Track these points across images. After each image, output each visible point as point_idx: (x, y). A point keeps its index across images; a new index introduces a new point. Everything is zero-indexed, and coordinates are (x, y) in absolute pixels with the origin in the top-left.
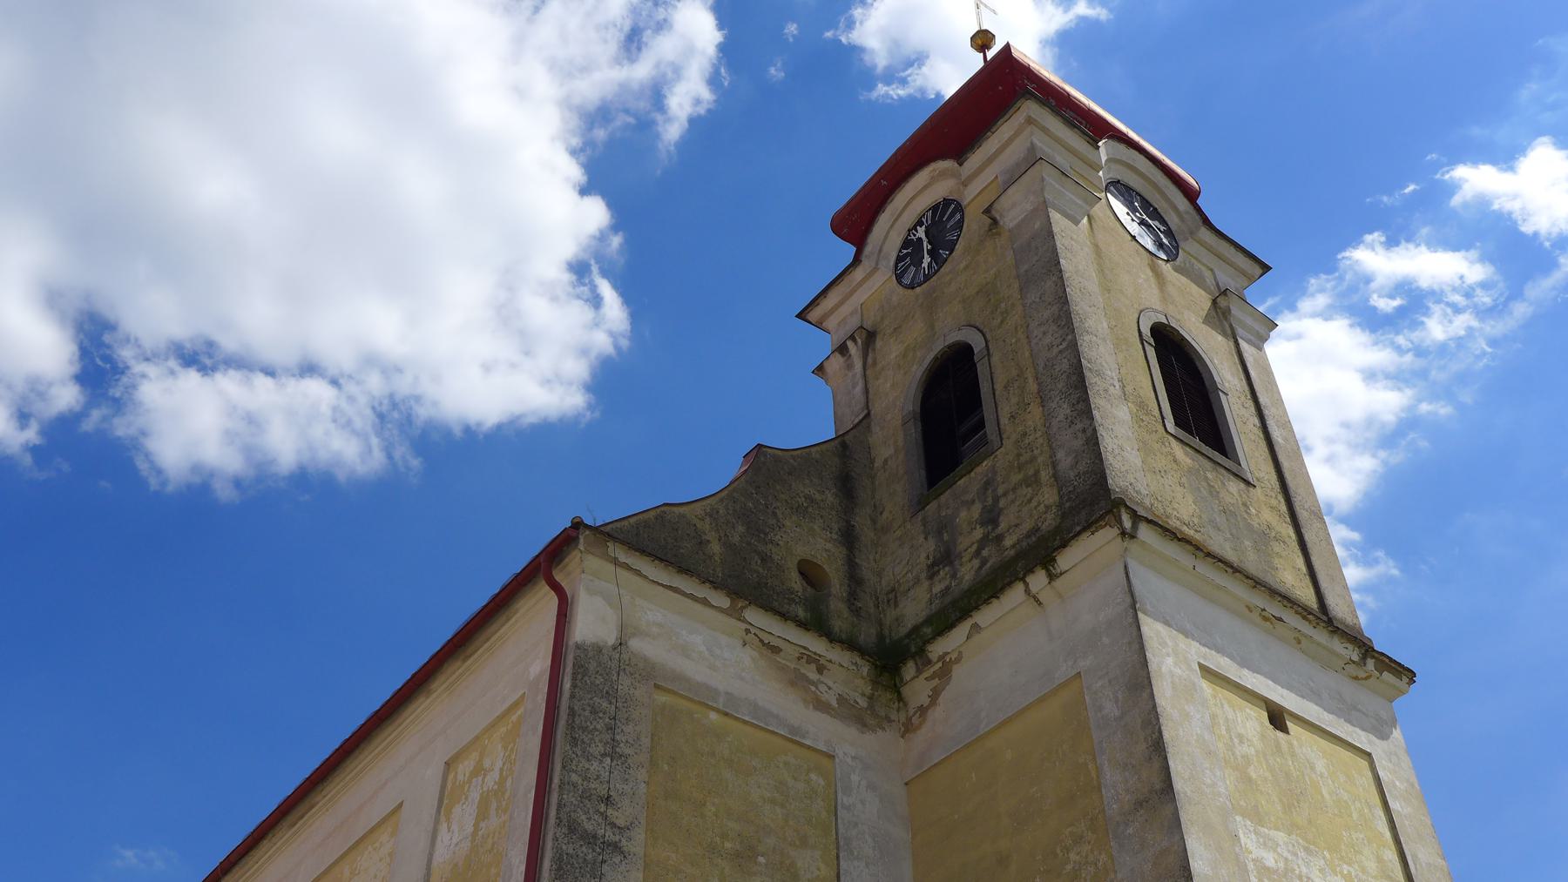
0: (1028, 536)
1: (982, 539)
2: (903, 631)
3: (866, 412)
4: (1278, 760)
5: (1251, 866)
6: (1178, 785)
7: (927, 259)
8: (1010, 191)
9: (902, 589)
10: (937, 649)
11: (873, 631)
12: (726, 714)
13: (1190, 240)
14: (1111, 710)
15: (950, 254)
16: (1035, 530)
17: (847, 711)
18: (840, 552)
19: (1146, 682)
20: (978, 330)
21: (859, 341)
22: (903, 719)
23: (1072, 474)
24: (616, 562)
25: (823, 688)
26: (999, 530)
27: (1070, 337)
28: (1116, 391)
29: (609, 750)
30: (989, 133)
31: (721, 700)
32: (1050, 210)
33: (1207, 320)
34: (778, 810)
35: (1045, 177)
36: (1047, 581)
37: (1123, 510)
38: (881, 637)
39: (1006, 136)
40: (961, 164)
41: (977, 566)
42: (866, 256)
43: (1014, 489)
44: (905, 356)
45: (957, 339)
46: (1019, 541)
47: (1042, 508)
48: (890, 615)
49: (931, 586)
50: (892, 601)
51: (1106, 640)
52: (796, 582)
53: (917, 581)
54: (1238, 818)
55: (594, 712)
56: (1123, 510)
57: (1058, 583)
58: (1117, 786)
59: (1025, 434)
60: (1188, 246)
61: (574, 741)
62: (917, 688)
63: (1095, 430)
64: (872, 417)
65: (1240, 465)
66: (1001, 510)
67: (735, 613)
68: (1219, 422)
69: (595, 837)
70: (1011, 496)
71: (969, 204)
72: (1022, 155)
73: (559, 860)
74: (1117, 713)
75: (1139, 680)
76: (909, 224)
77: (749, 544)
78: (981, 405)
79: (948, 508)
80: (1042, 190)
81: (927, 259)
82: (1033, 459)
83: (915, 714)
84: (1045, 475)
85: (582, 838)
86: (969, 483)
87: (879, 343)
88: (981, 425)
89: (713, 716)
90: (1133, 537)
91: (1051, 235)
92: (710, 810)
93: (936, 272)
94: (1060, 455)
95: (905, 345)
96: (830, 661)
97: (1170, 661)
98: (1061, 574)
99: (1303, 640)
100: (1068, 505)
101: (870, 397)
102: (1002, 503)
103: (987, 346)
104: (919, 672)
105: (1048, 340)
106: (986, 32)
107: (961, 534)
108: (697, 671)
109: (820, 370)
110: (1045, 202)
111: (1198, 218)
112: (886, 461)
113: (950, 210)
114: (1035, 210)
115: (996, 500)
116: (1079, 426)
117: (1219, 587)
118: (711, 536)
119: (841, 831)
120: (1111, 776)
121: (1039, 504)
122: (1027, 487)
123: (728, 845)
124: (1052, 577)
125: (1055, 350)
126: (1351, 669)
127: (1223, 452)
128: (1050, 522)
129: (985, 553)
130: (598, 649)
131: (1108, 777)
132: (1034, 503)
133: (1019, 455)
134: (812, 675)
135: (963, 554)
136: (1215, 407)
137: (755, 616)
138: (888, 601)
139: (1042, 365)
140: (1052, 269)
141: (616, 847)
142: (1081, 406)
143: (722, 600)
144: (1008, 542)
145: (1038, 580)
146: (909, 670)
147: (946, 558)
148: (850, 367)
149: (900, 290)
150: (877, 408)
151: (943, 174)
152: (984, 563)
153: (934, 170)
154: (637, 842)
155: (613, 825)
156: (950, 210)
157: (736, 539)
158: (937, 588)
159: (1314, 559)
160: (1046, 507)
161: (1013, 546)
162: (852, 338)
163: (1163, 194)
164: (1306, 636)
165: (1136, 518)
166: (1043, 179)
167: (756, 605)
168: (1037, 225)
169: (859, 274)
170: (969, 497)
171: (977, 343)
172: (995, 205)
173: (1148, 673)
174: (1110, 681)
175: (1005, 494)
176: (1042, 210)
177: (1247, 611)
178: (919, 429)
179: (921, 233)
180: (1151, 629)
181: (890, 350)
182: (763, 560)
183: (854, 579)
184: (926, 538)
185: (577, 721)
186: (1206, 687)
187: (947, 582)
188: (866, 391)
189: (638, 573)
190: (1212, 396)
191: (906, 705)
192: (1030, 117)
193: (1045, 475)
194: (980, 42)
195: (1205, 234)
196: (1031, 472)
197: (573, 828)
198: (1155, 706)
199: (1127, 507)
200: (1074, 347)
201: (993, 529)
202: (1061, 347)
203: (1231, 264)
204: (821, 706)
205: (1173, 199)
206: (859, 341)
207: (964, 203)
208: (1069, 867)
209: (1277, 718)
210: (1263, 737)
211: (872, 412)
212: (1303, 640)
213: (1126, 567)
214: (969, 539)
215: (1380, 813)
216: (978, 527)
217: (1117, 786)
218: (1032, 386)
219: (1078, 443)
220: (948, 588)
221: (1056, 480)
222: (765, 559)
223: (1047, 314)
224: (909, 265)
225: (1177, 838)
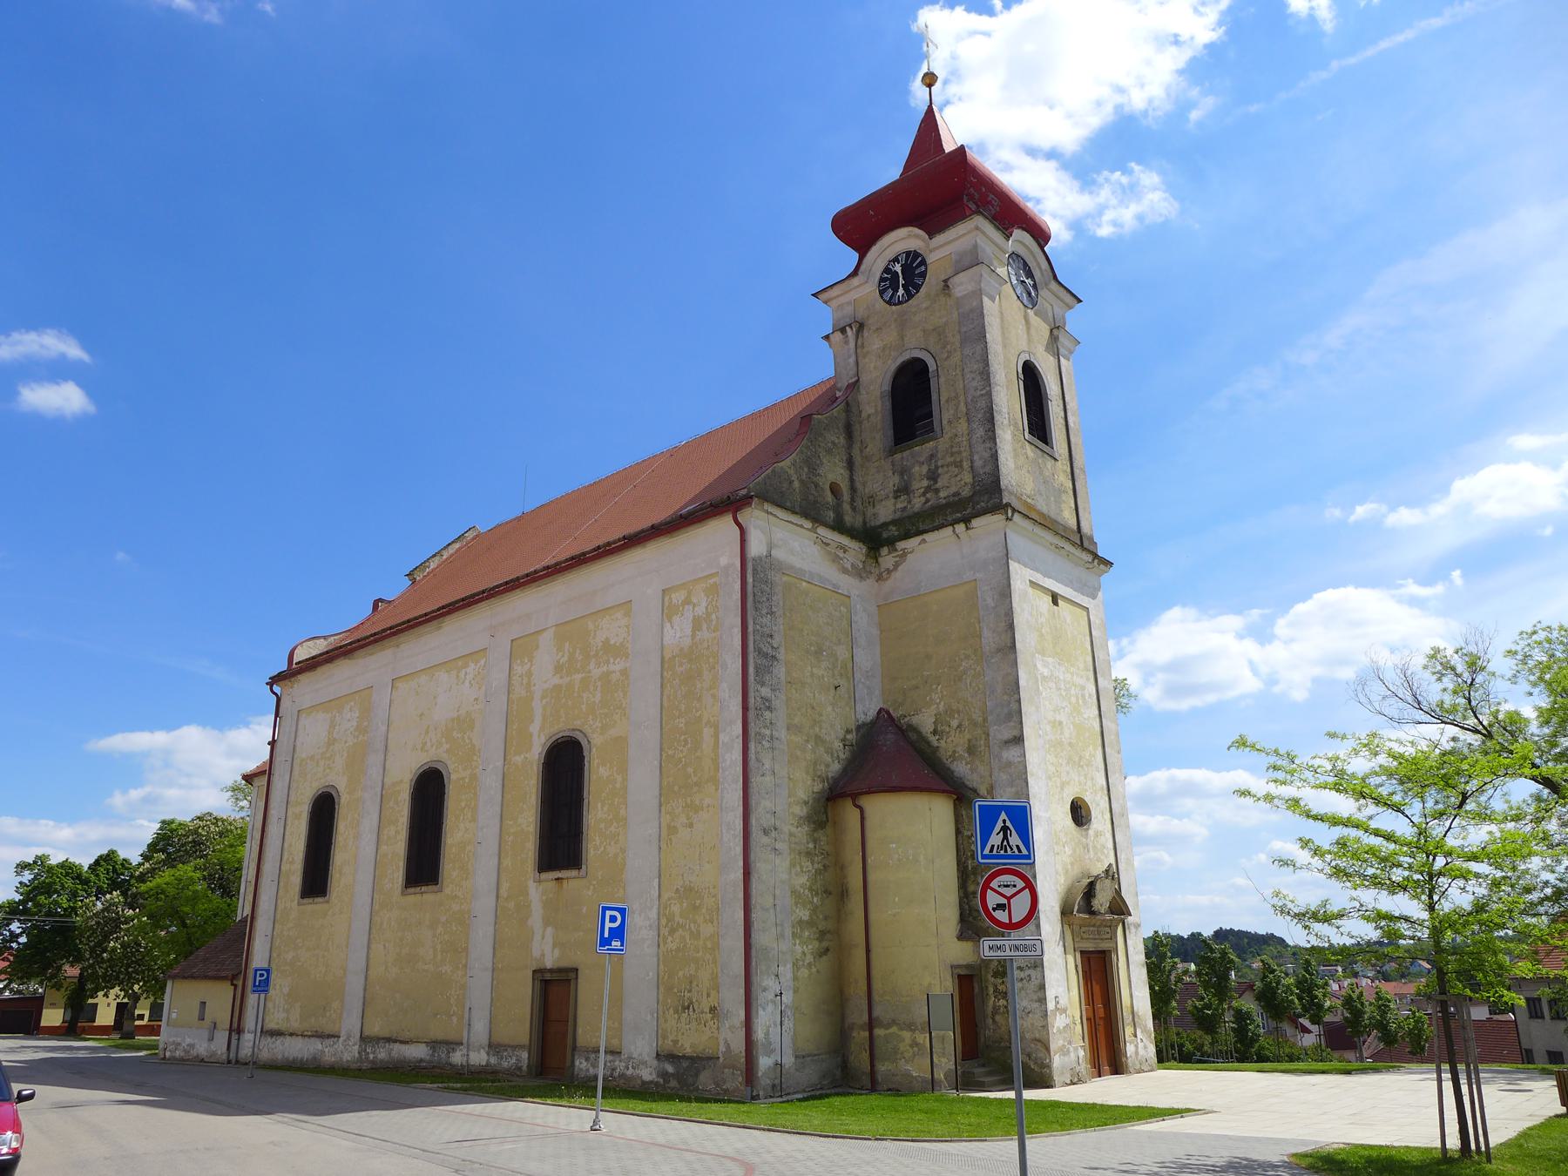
0: (954, 495)
1: (928, 487)
3: (857, 378)
5: (1039, 677)
6: (1018, 645)
7: (901, 291)
8: (961, 275)
10: (901, 545)
11: (861, 520)
13: (1045, 289)
15: (917, 293)
16: (956, 494)
17: (860, 573)
18: (846, 474)
21: (854, 329)
26: (937, 486)
28: (1006, 422)
33: (1047, 349)
38: (865, 523)
39: (961, 233)
40: (931, 239)
43: (948, 466)
46: (948, 496)
47: (963, 482)
48: (870, 511)
51: (991, 568)
53: (887, 497)
58: (989, 639)
60: (1043, 293)
61: (756, 609)
62: (887, 559)
63: (996, 451)
67: (813, 530)
70: (946, 469)
74: (993, 605)
76: (892, 256)
80: (980, 281)
82: (960, 453)
84: (966, 465)
86: (923, 450)
87: (866, 334)
88: (930, 415)
89: (804, 584)
90: (1011, 520)
92: (1186, 972)
93: (907, 301)
94: (976, 457)
97: (1019, 582)
100: (978, 488)
102: (940, 471)
104: (890, 553)
105: (975, 384)
106: (933, 74)
107: (915, 479)
108: (796, 562)
109: (827, 338)
111: (1051, 274)
113: (918, 261)
114: (973, 292)
115: (937, 467)
116: (988, 445)
118: (794, 478)
120: (986, 633)
121: (961, 480)
124: (967, 528)
125: (979, 393)
129: (928, 495)
130: (760, 558)
132: (958, 478)
134: (841, 555)
136: (1045, 409)
138: (869, 502)
141: (774, 657)
142: (990, 433)
143: (808, 524)
144: (942, 494)
145: (960, 528)
146: (885, 551)
148: (846, 343)
149: (881, 304)
150: (864, 378)
151: (917, 236)
152: (927, 501)
153: (912, 231)
154: (781, 655)
156: (918, 261)
157: (804, 477)
158: (900, 506)
160: (965, 483)
162: (850, 326)
165: (1014, 510)
166: (981, 275)
168: (975, 304)
169: (855, 281)
170: (922, 459)
171: (932, 366)
175: (942, 466)
179: (898, 268)
180: (1013, 566)
183: (853, 489)
184: (894, 474)
186: (1030, 590)
187: (906, 504)
188: (857, 363)
189: (775, 516)
193: (966, 465)
195: (1053, 285)
196: (958, 460)
197: (759, 651)
200: (989, 395)
203: (1062, 301)
204: (845, 571)
206: (854, 329)
207: (928, 262)
208: (961, 668)
213: (1005, 534)
214: (920, 485)
217: (989, 639)
218: (963, 408)
219: (987, 455)
220: (905, 507)
222: (816, 486)
224: (888, 288)
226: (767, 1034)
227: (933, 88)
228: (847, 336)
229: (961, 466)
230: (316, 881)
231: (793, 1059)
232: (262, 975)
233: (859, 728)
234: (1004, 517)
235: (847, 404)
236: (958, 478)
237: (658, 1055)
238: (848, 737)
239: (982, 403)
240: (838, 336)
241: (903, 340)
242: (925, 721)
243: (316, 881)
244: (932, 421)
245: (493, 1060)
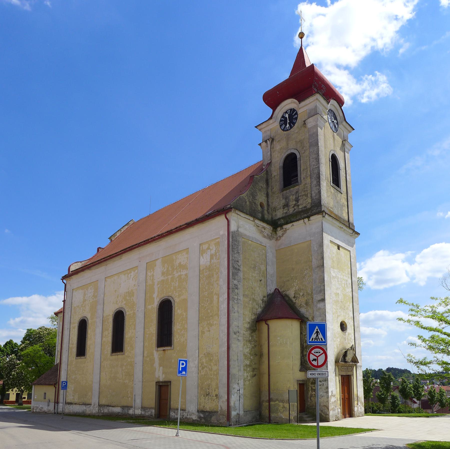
2: (277, 218)
3: (271, 161)
7: (288, 125)
8: (310, 118)
9: (277, 208)
10: (285, 227)
11: (271, 217)
12: (252, 241)
14: (316, 249)
16: (305, 207)
18: (266, 199)
19: (322, 246)
20: (298, 152)
21: (270, 141)
22: (276, 237)
23: (315, 198)
24: (237, 214)
25: (265, 233)
26: (298, 204)
27: (318, 165)
30: (307, 99)
31: (251, 238)
32: (318, 127)
34: (259, 258)
35: (318, 118)
36: (308, 221)
37: (324, 212)
38: (272, 218)
39: (311, 101)
41: (293, 210)
42: (274, 118)
44: (281, 149)
45: (294, 152)
46: (302, 208)
49: (283, 210)
50: (275, 210)
51: (317, 235)
53: (280, 208)
54: (331, 268)
56: (324, 212)
57: (309, 221)
58: (315, 263)
59: (306, 184)
61: (233, 251)
62: (280, 232)
63: (320, 190)
64: (272, 163)
65: (341, 189)
66: (299, 199)
67: (254, 221)
68: (339, 184)
70: (302, 197)
71: (299, 114)
72: (314, 107)
73: (233, 273)
75: (321, 245)
79: (288, 194)
80: (317, 121)
81: (288, 125)
82: (307, 191)
83: (279, 237)
84: (309, 195)
86: (294, 189)
89: (250, 242)
91: (317, 135)
93: (290, 129)
94: (313, 192)
95: (281, 147)
96: (266, 228)
97: (326, 241)
98: (311, 220)
99: (345, 231)
100: (313, 204)
101: (272, 157)
102: (300, 198)
103: (300, 157)
104: (281, 230)
105: (314, 163)
107: (290, 201)
108: (247, 233)
109: (260, 144)
110: (317, 125)
111: (344, 118)
112: (275, 176)
114: (315, 126)
115: (299, 197)
116: (317, 188)
118: (247, 200)
119: (267, 261)
120: (314, 260)
122: (305, 196)
123: (252, 266)
124: (309, 220)
125: (315, 167)
126: (351, 234)
127: (339, 187)
128: (309, 206)
129: (295, 207)
130: (235, 232)
131: (313, 260)
132: (306, 201)
133: (304, 188)
135: (291, 206)
138: (274, 210)
139: (312, 169)
140: (317, 145)
142: (318, 183)
144: (300, 207)
145: (306, 220)
146: (279, 229)
147: (286, 205)
148: (267, 146)
150: (273, 161)
151: (294, 102)
152: (295, 210)
155: (238, 266)
158: (285, 211)
159: (349, 209)
161: (301, 208)
162: (269, 140)
163: (338, 111)
164: (345, 230)
165: (326, 213)
166: (318, 119)
167: (257, 219)
169: (271, 121)
172: (306, 121)
173: (323, 244)
174: (316, 243)
175: (301, 196)
176: (316, 126)
177: (338, 227)
179: (287, 116)
181: (278, 146)
182: (255, 204)
183: (268, 205)
184: (283, 199)
187: (287, 211)
190: (338, 170)
191: (277, 234)
192: (317, 98)
193: (309, 195)
194: (301, 36)
195: (344, 123)
196: (306, 193)
198: (323, 251)
199: (325, 212)
200: (319, 167)
201: (297, 203)
202: (316, 167)
204: (264, 237)
205: (340, 113)
206: (270, 141)
209: (339, 247)
211: (272, 161)
212: (345, 231)
215: (350, 262)
216: (294, 201)
217: (315, 263)
219: (317, 191)
220: (287, 212)
221: (311, 197)
223: (314, 156)
224: (283, 124)
225: (323, 274)
231: (243, 412)
232: (64, 384)
233: (268, 295)
235: (267, 171)
237: (198, 411)
238: (264, 299)
239: (316, 171)
242: (291, 293)
245: (143, 413)
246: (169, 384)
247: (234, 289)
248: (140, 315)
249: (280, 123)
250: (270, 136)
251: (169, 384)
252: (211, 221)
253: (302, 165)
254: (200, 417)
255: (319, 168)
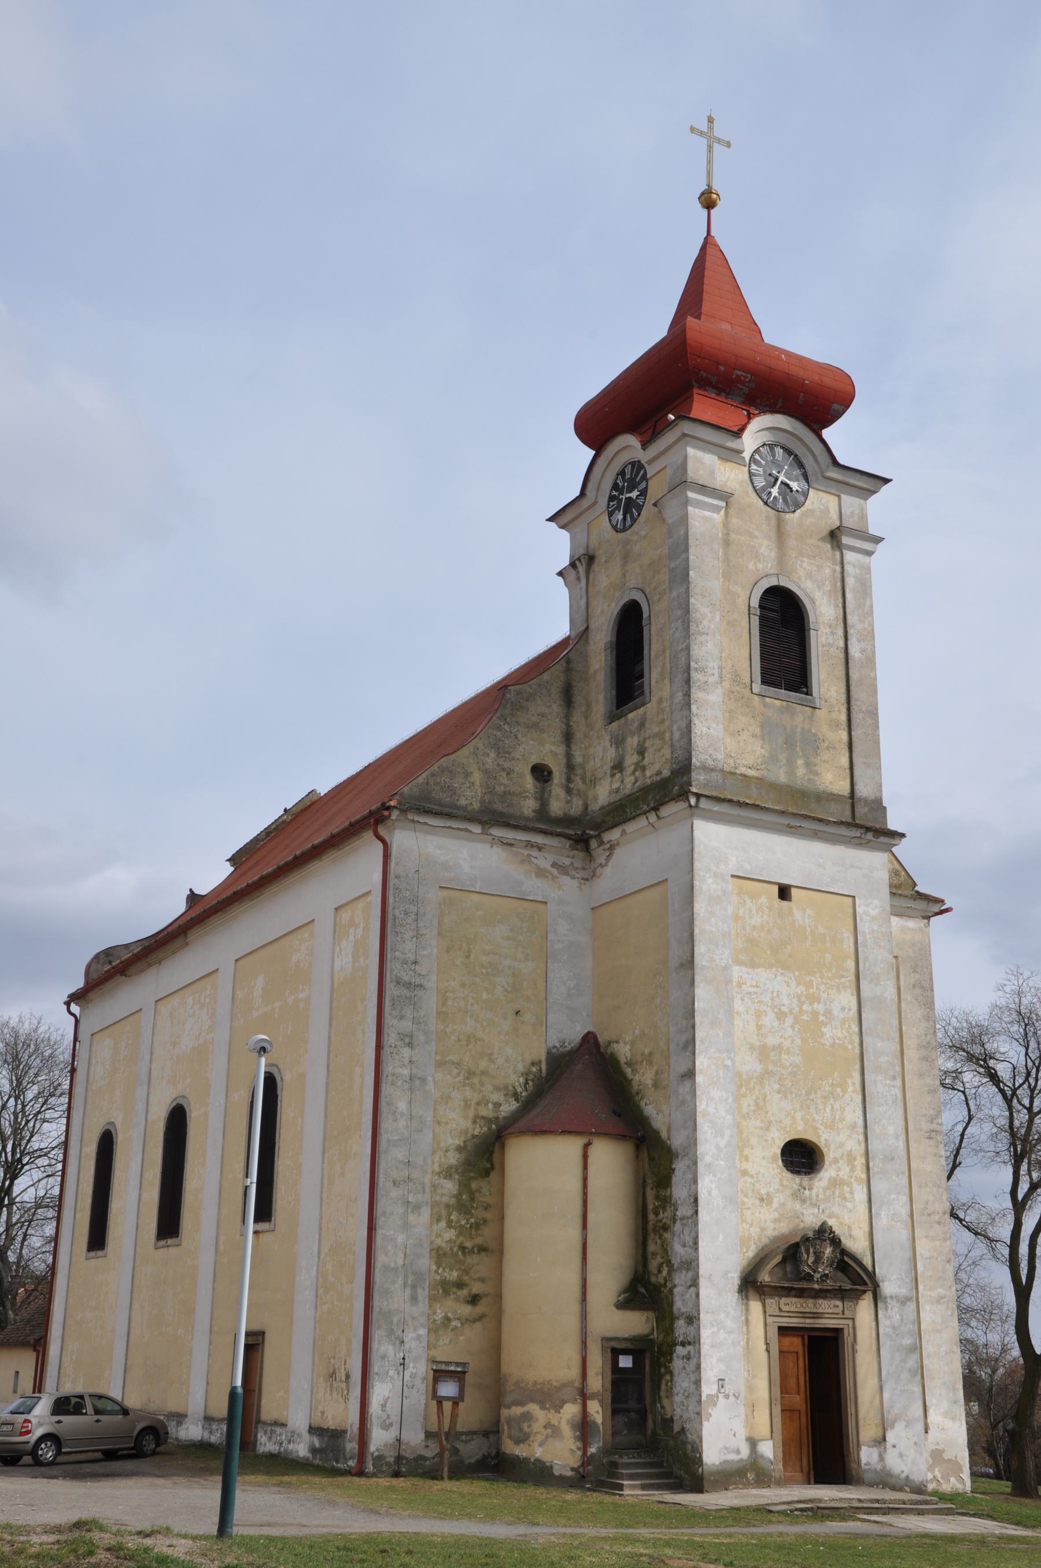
3: (586, 625)
4: (50, 1454)
11: (581, 803)
18: (561, 750)
24: (413, 821)
29: (415, 932)
38: (586, 807)
52: (529, 782)
55: (406, 913)
69: (410, 984)
77: (498, 765)
78: (642, 659)
85: (404, 985)
117: (757, 819)
129: (637, 774)
137: (498, 832)
143: (476, 829)
144: (648, 773)
145: (652, 817)
147: (618, 767)
148: (578, 579)
150: (593, 626)
152: (636, 781)
158: (615, 786)
178: (614, 657)
182: (508, 774)
183: (570, 767)
185: (397, 921)
189: (426, 824)
210: (770, 908)
222: (509, 772)
226: (384, 1406)
227: (712, 211)
228: (578, 572)
229: (663, 739)
230: (97, 1239)
234: (687, 805)
235: (568, 662)
236: (661, 754)
237: (310, 1427)
239: (683, 661)
240: (572, 573)
241: (625, 576)
242: (623, 1051)
243: (97, 1239)
244: (643, 682)
245: (206, 1435)
246: (260, 1338)
247: (399, 1047)
248: (215, 1121)
249: (608, 508)
250: (587, 547)
251: (260, 1338)
252: (357, 843)
253: (654, 642)
254: (314, 1450)
255: (689, 650)
